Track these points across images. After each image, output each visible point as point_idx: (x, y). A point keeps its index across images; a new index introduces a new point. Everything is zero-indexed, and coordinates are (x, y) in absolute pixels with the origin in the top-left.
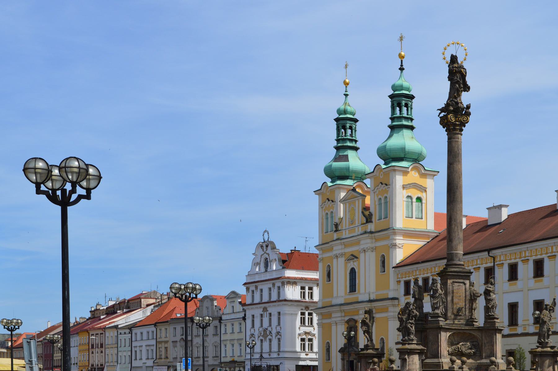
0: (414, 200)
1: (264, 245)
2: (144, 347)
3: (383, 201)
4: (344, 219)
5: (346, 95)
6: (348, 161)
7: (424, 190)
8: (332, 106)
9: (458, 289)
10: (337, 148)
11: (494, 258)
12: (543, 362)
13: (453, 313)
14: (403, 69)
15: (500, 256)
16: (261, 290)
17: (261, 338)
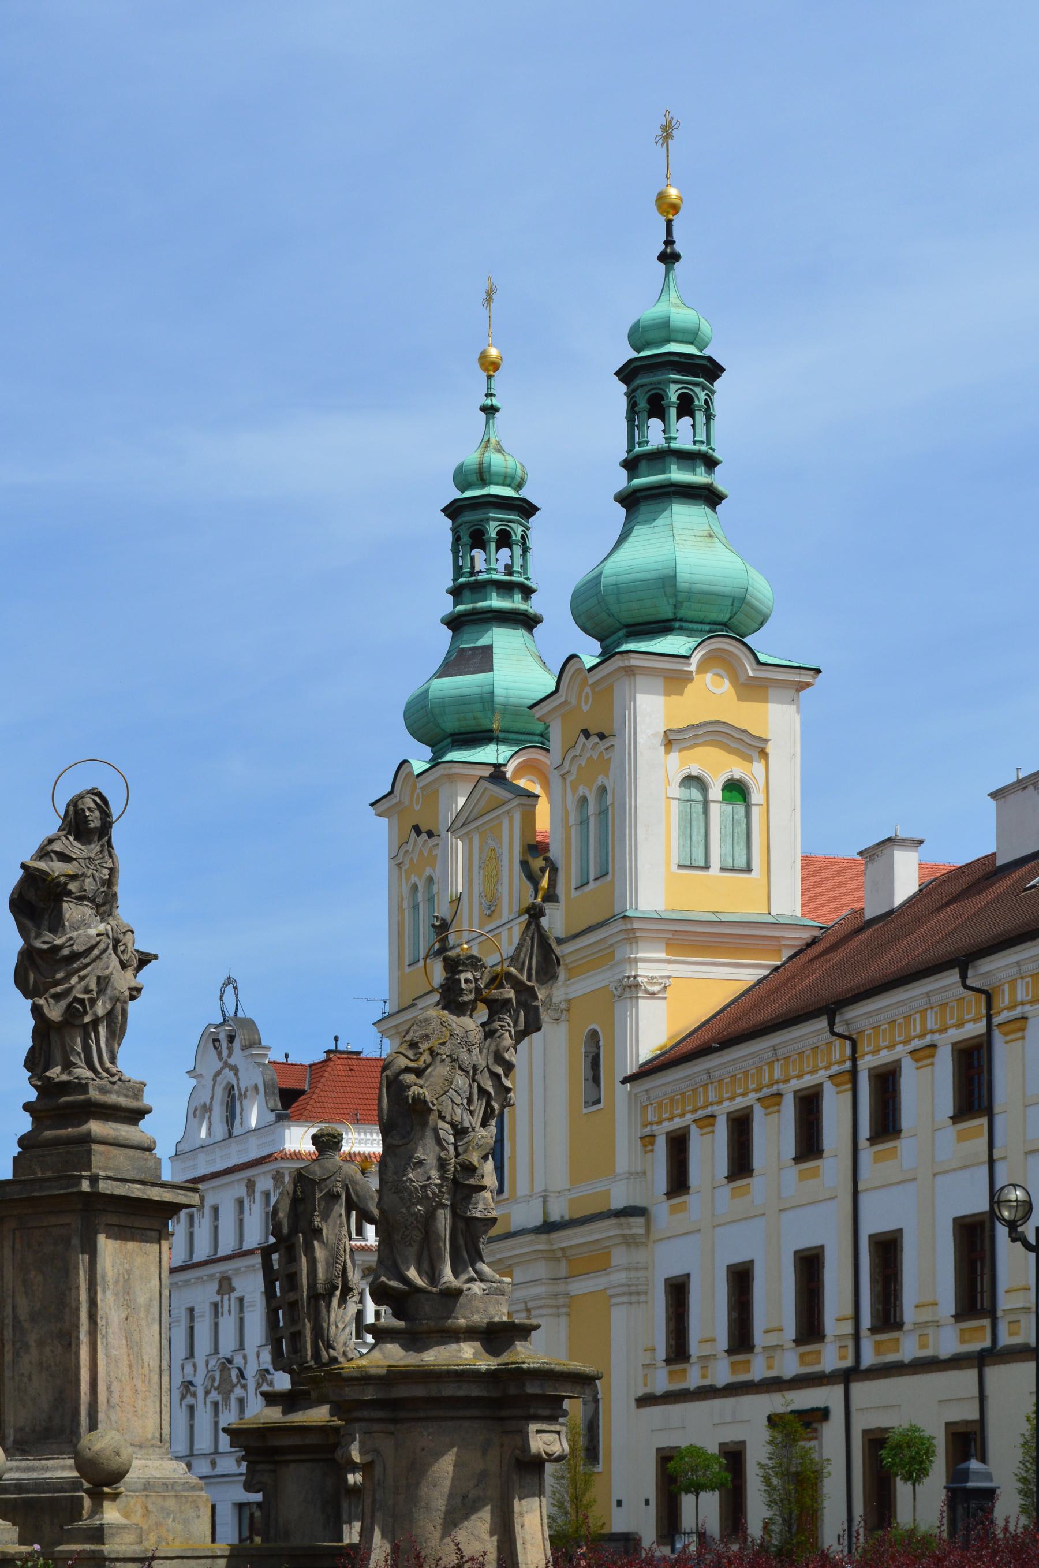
0: (715, 792)
1: (222, 1036)
3: (592, 808)
4: (465, 901)
5: (490, 411)
6: (491, 670)
7: (756, 748)
8: (426, 453)
10: (455, 623)
11: (989, 997)
12: (416, 1470)
14: (675, 257)
15: (1013, 984)
16: (216, 1210)
17: (214, 1395)
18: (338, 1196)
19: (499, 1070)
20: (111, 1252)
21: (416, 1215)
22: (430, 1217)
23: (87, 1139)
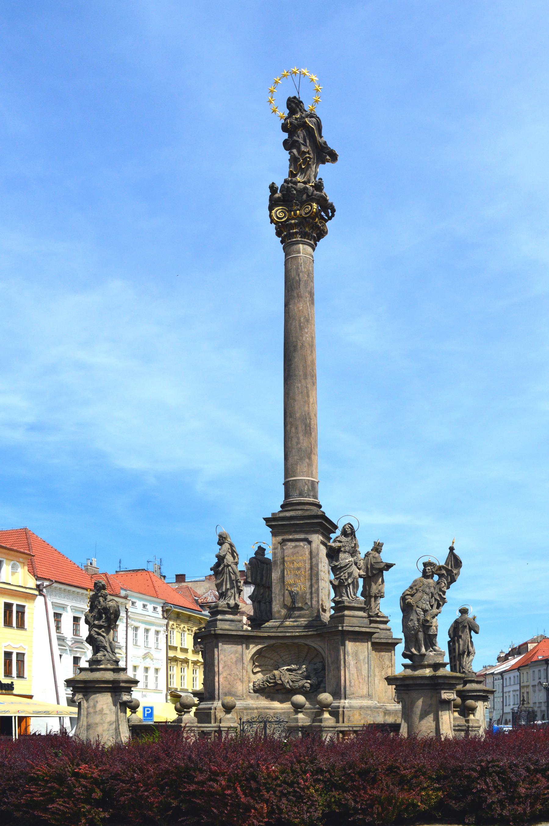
2: (511, 692)
9: (293, 554)
13: (285, 606)
18: (466, 626)
19: (441, 594)
20: (350, 646)
21: (412, 634)
22: (416, 634)
23: (344, 616)
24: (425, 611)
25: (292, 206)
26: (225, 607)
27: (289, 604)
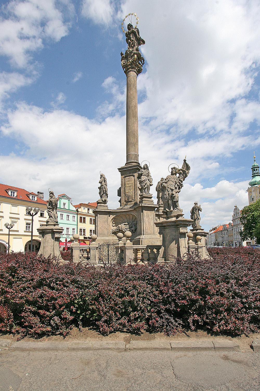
18: (197, 209)
22: (168, 201)
24: (172, 190)
25: (128, 59)
26: (101, 201)
27: (126, 200)
